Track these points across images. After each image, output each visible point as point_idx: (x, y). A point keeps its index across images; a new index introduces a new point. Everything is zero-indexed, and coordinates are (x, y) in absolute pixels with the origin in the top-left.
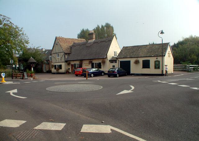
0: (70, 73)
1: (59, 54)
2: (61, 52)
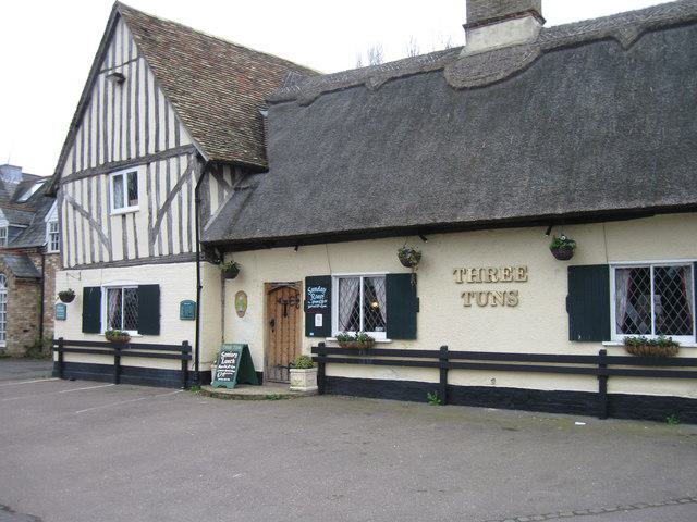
1: (141, 170)
2: (158, 157)
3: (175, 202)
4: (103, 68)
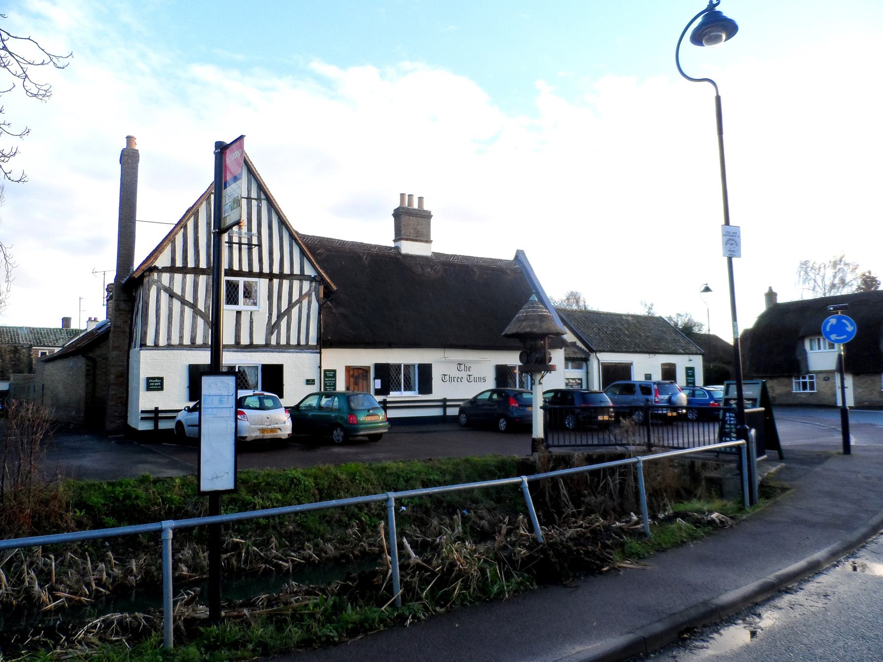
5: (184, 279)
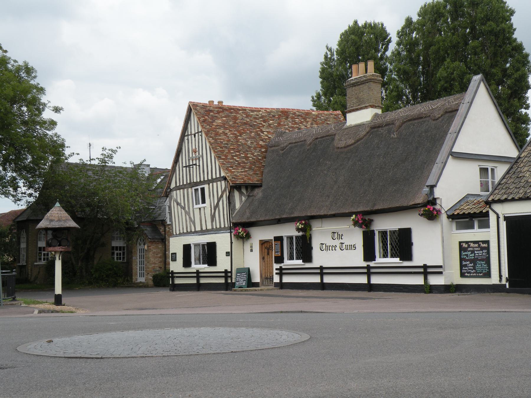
0: (256, 285)
1: (206, 187)
3: (221, 203)
4: (186, 134)
5: (180, 192)
